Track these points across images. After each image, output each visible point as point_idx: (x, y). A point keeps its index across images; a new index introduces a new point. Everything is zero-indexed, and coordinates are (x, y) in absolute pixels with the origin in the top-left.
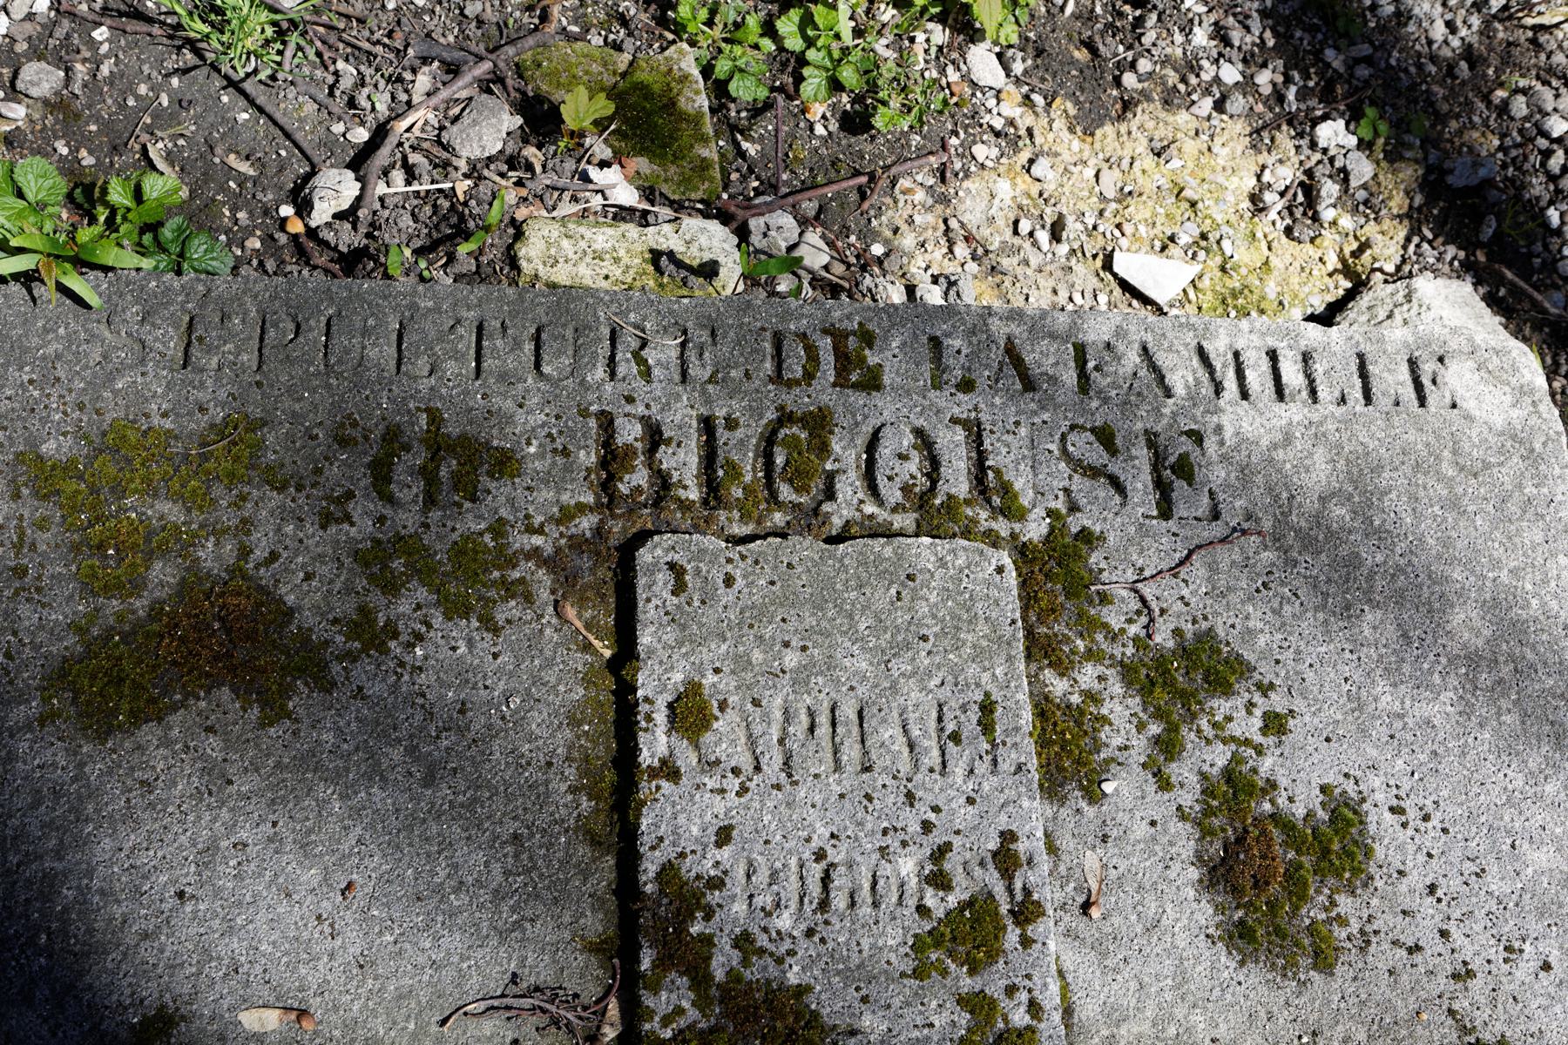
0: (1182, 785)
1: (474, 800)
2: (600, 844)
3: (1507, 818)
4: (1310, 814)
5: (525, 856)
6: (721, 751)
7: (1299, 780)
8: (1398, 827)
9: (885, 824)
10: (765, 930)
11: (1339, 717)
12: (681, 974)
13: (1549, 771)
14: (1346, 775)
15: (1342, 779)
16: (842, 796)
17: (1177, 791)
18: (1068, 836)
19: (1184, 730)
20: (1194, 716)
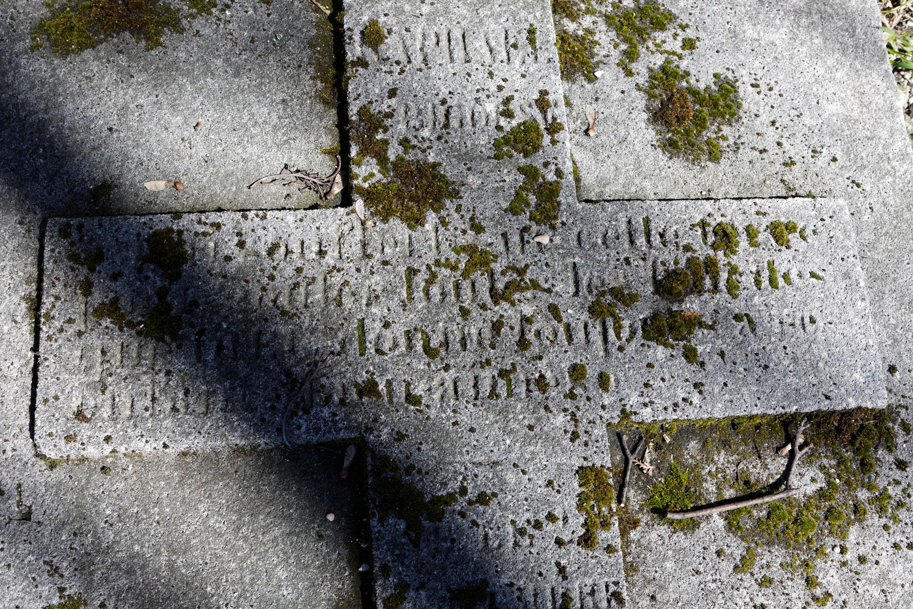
0: (638, 74)
1: (261, 83)
2: (328, 103)
3: (815, 89)
4: (708, 88)
5: (289, 110)
6: (390, 53)
7: (701, 72)
8: (756, 94)
9: (478, 87)
10: (416, 137)
11: (724, 41)
12: (372, 158)
13: (839, 66)
14: (728, 69)
15: (725, 71)
16: (454, 74)
17: (636, 76)
18: (577, 98)
19: (640, 47)
20: (645, 40)
